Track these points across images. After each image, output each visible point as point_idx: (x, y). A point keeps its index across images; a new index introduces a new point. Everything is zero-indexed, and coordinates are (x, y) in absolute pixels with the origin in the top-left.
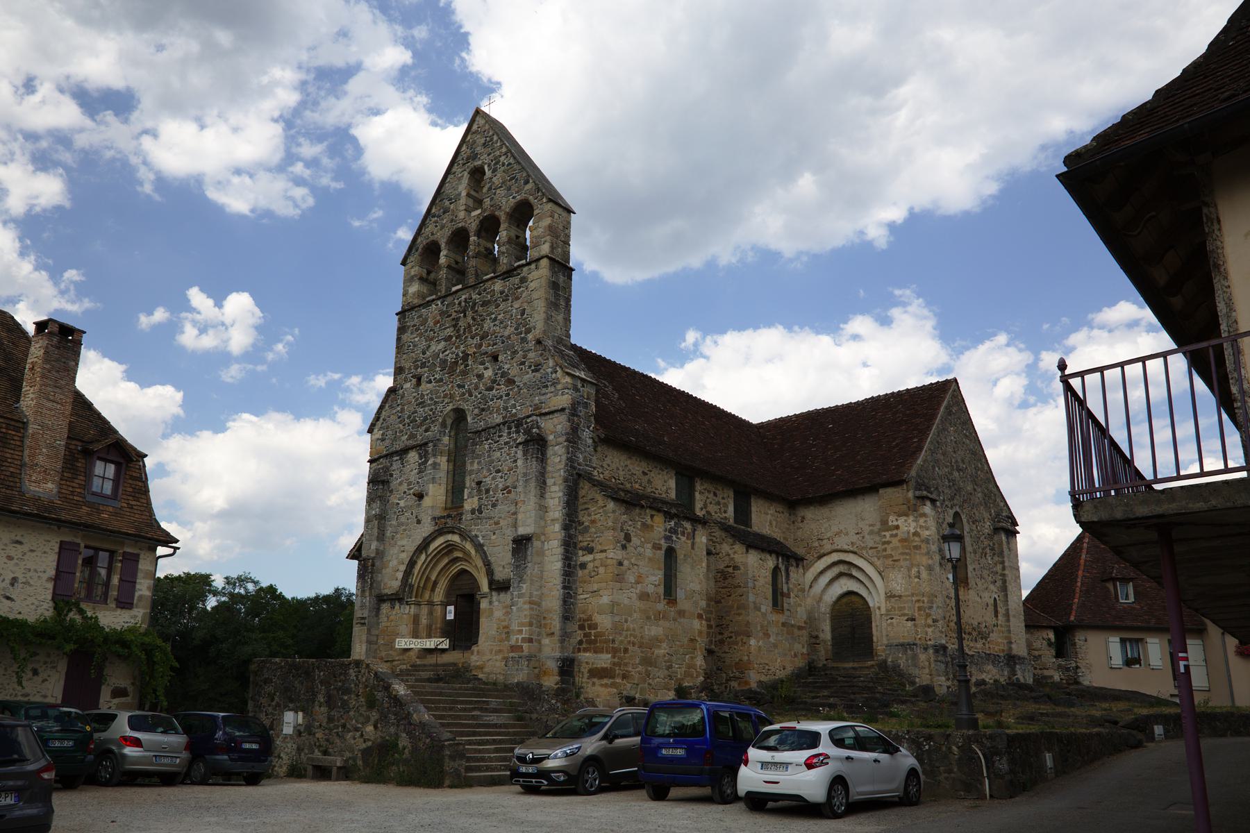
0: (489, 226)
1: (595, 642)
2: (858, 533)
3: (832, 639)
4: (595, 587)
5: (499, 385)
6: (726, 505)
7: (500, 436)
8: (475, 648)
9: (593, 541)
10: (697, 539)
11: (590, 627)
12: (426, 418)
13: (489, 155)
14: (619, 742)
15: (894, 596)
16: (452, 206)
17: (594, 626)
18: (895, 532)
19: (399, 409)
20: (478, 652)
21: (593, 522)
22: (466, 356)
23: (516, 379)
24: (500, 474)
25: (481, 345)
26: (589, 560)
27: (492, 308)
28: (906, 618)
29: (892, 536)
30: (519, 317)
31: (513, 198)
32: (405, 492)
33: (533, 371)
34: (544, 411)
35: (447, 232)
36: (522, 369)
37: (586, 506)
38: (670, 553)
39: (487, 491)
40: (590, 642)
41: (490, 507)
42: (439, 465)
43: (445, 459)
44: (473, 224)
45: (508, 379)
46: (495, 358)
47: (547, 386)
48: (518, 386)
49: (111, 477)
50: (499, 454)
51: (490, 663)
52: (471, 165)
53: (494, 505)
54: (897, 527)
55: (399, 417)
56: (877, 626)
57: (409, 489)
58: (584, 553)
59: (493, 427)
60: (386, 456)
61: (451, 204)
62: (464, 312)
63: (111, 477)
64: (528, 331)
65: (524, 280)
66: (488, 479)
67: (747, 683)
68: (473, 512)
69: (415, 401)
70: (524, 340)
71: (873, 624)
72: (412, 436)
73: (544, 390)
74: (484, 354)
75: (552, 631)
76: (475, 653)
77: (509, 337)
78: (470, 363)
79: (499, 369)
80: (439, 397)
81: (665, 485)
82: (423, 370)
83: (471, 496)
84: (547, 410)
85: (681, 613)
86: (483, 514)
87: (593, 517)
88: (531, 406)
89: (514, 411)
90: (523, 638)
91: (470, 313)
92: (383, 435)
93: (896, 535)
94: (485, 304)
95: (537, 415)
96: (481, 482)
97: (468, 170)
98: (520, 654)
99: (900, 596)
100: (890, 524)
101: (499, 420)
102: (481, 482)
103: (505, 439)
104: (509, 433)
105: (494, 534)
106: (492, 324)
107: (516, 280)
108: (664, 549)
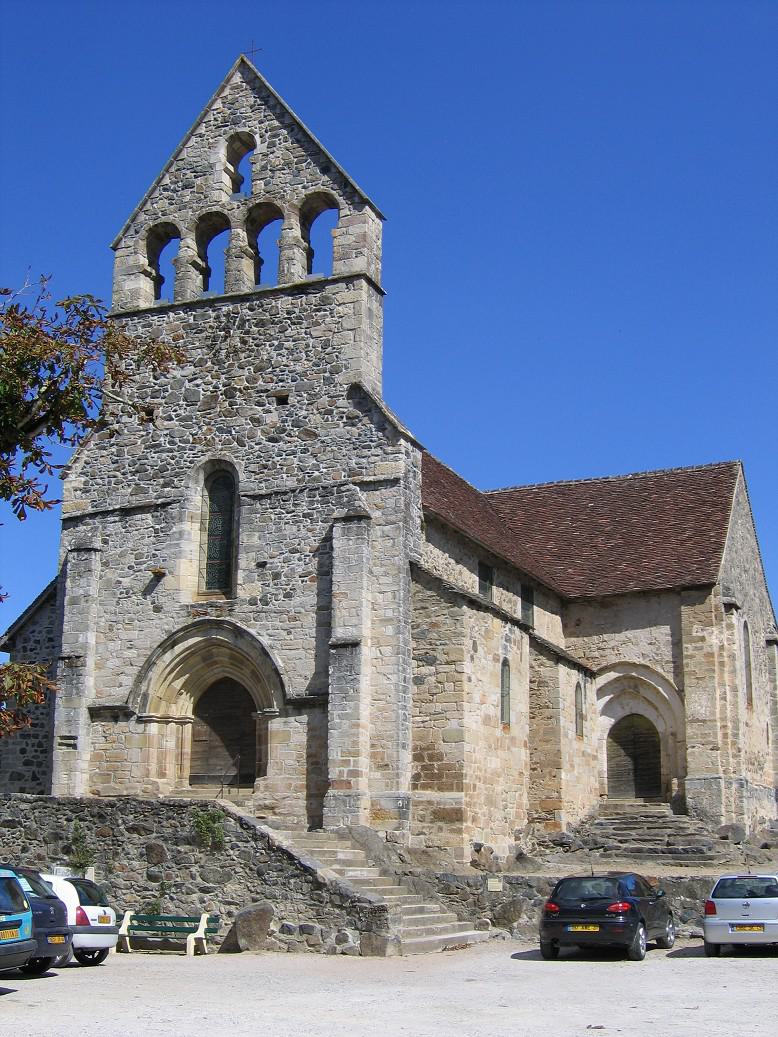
0: (263, 217)
1: (440, 776)
2: (650, 644)
3: (51, 749)
4: (439, 707)
5: (289, 435)
6: (515, 605)
7: (295, 505)
8: (259, 782)
9: (434, 650)
10: (524, 650)
11: (431, 758)
12: (163, 469)
13: (261, 122)
14: (26, 906)
15: (698, 720)
16: (198, 181)
17: (440, 757)
18: (700, 644)
19: (114, 449)
20: (266, 787)
21: (434, 625)
22: (230, 394)
23: (318, 432)
24: (298, 555)
25: (255, 380)
26: (427, 672)
27: (273, 331)
28: (711, 746)
29: (696, 648)
30: (320, 349)
31: (304, 187)
32: (130, 568)
33: (345, 424)
34: (367, 479)
35: (191, 215)
36: (327, 420)
37: (423, 605)
38: (505, 663)
39: (276, 576)
40: (432, 776)
41: (281, 597)
42: (189, 534)
43: (197, 526)
44: (236, 212)
45: (306, 430)
46: (282, 400)
47: (369, 447)
48: (323, 442)
49: (663, 633)
50: (295, 528)
51: (287, 802)
52: (231, 131)
53: (288, 596)
54: (703, 639)
55: (116, 462)
56: (668, 755)
57: (140, 564)
58: (421, 663)
59: (285, 493)
60: (93, 516)
61: (196, 177)
62: (226, 329)
63: (663, 633)
64: (336, 371)
65: (325, 301)
66: (276, 560)
67: (557, 825)
68: (253, 602)
69: (143, 442)
70: (329, 381)
71: (663, 753)
72: (139, 490)
73: (366, 452)
74: (262, 391)
75: (386, 761)
76: (262, 788)
77: (304, 374)
78: (238, 402)
79: (290, 415)
80: (187, 442)
81: (468, 580)
82: (156, 400)
83: (249, 580)
84: (371, 478)
85: (513, 739)
86: (271, 607)
87: (434, 619)
88: (344, 470)
89: (316, 473)
90: (349, 770)
91: (236, 333)
92: (86, 483)
93: (702, 648)
94: (261, 324)
95: (355, 484)
96: (265, 563)
97: (226, 137)
98: (348, 792)
99: (704, 721)
100: (694, 634)
101: (291, 483)
102: (265, 563)
103: (304, 508)
104: (311, 503)
105: (289, 633)
106: (274, 354)
107: (314, 299)
108: (501, 661)
